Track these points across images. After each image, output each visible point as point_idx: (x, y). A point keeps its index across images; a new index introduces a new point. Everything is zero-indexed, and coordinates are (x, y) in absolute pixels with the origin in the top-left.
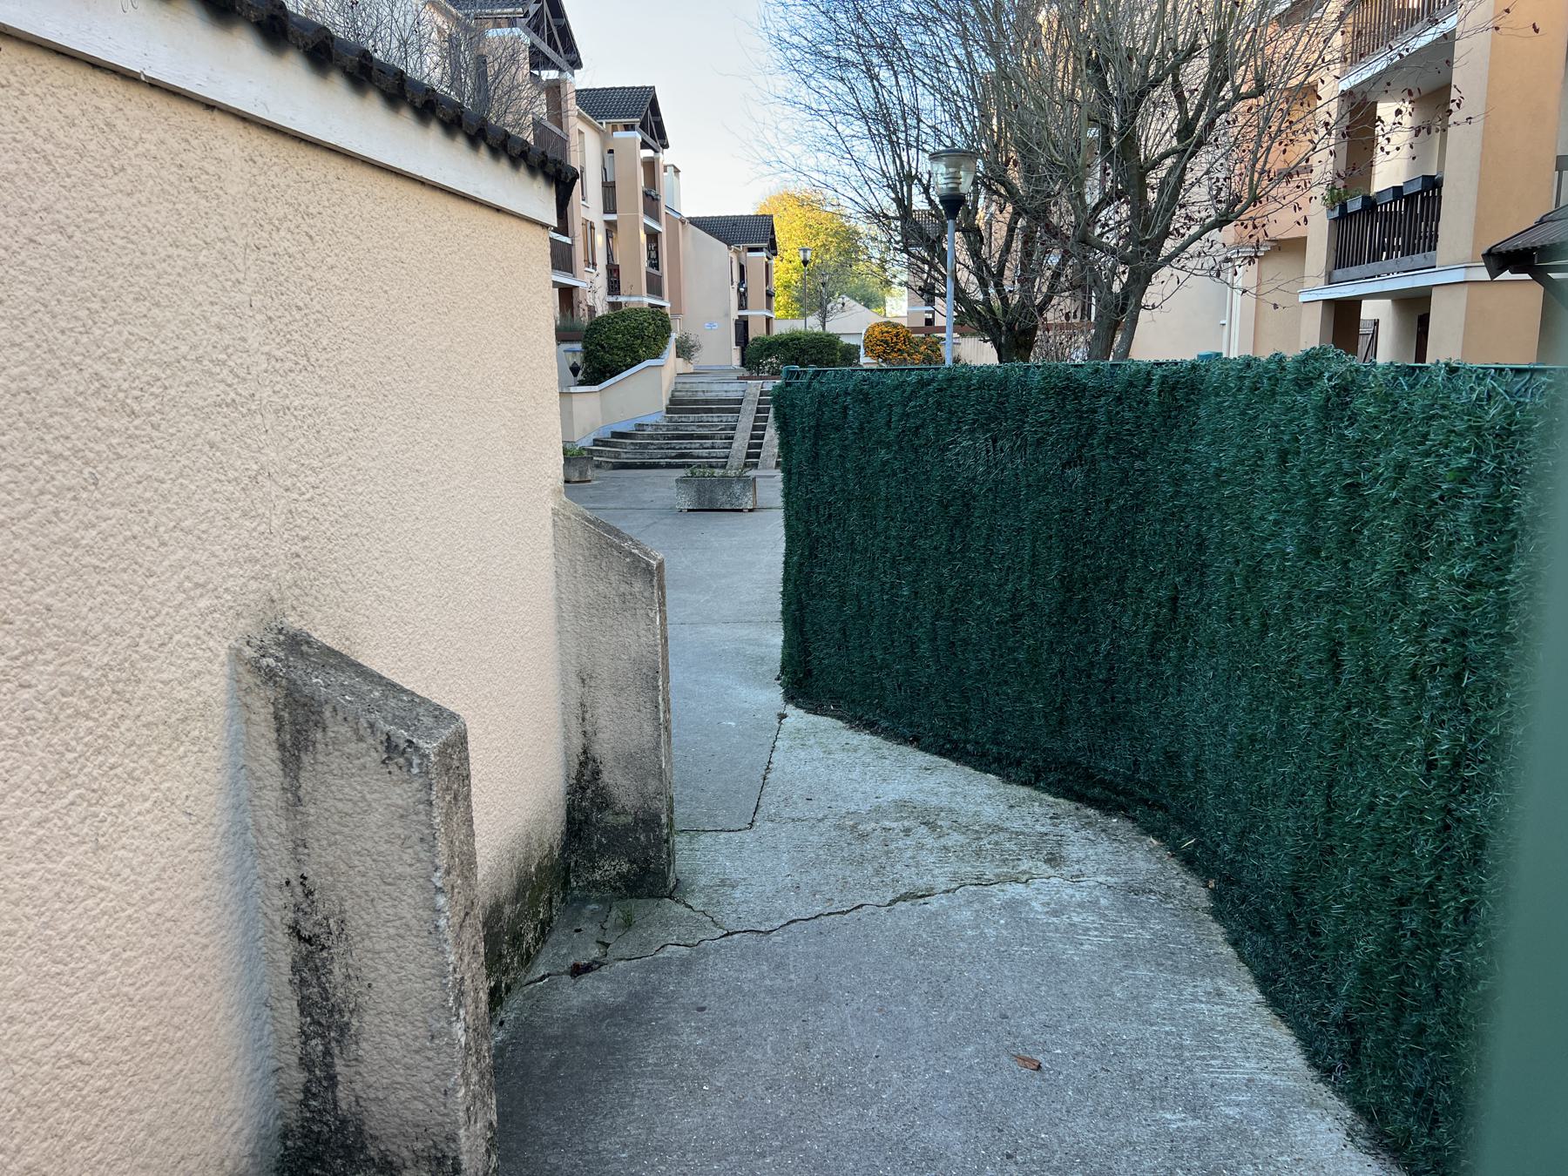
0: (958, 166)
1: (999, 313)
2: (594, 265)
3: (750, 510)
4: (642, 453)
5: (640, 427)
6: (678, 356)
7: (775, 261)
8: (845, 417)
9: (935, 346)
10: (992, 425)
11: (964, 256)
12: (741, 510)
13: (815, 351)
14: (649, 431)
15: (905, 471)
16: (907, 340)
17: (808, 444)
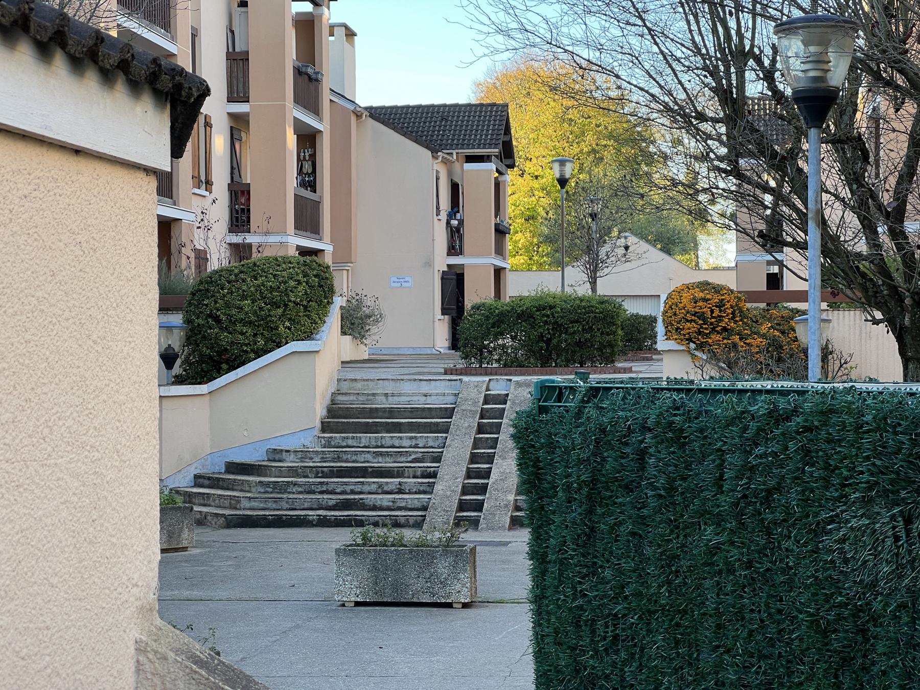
0: (824, 43)
1: (898, 278)
2: (209, 184)
3: (465, 606)
4: (276, 500)
5: (276, 454)
6: (344, 333)
7: (511, 176)
8: (643, 469)
9: (786, 324)
10: (903, 494)
11: (833, 180)
12: (449, 605)
13: (577, 327)
14: (290, 462)
15: (749, 565)
16: (738, 313)
17: (576, 512)
